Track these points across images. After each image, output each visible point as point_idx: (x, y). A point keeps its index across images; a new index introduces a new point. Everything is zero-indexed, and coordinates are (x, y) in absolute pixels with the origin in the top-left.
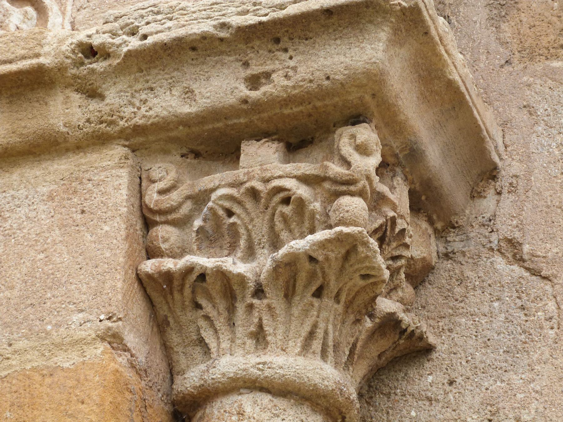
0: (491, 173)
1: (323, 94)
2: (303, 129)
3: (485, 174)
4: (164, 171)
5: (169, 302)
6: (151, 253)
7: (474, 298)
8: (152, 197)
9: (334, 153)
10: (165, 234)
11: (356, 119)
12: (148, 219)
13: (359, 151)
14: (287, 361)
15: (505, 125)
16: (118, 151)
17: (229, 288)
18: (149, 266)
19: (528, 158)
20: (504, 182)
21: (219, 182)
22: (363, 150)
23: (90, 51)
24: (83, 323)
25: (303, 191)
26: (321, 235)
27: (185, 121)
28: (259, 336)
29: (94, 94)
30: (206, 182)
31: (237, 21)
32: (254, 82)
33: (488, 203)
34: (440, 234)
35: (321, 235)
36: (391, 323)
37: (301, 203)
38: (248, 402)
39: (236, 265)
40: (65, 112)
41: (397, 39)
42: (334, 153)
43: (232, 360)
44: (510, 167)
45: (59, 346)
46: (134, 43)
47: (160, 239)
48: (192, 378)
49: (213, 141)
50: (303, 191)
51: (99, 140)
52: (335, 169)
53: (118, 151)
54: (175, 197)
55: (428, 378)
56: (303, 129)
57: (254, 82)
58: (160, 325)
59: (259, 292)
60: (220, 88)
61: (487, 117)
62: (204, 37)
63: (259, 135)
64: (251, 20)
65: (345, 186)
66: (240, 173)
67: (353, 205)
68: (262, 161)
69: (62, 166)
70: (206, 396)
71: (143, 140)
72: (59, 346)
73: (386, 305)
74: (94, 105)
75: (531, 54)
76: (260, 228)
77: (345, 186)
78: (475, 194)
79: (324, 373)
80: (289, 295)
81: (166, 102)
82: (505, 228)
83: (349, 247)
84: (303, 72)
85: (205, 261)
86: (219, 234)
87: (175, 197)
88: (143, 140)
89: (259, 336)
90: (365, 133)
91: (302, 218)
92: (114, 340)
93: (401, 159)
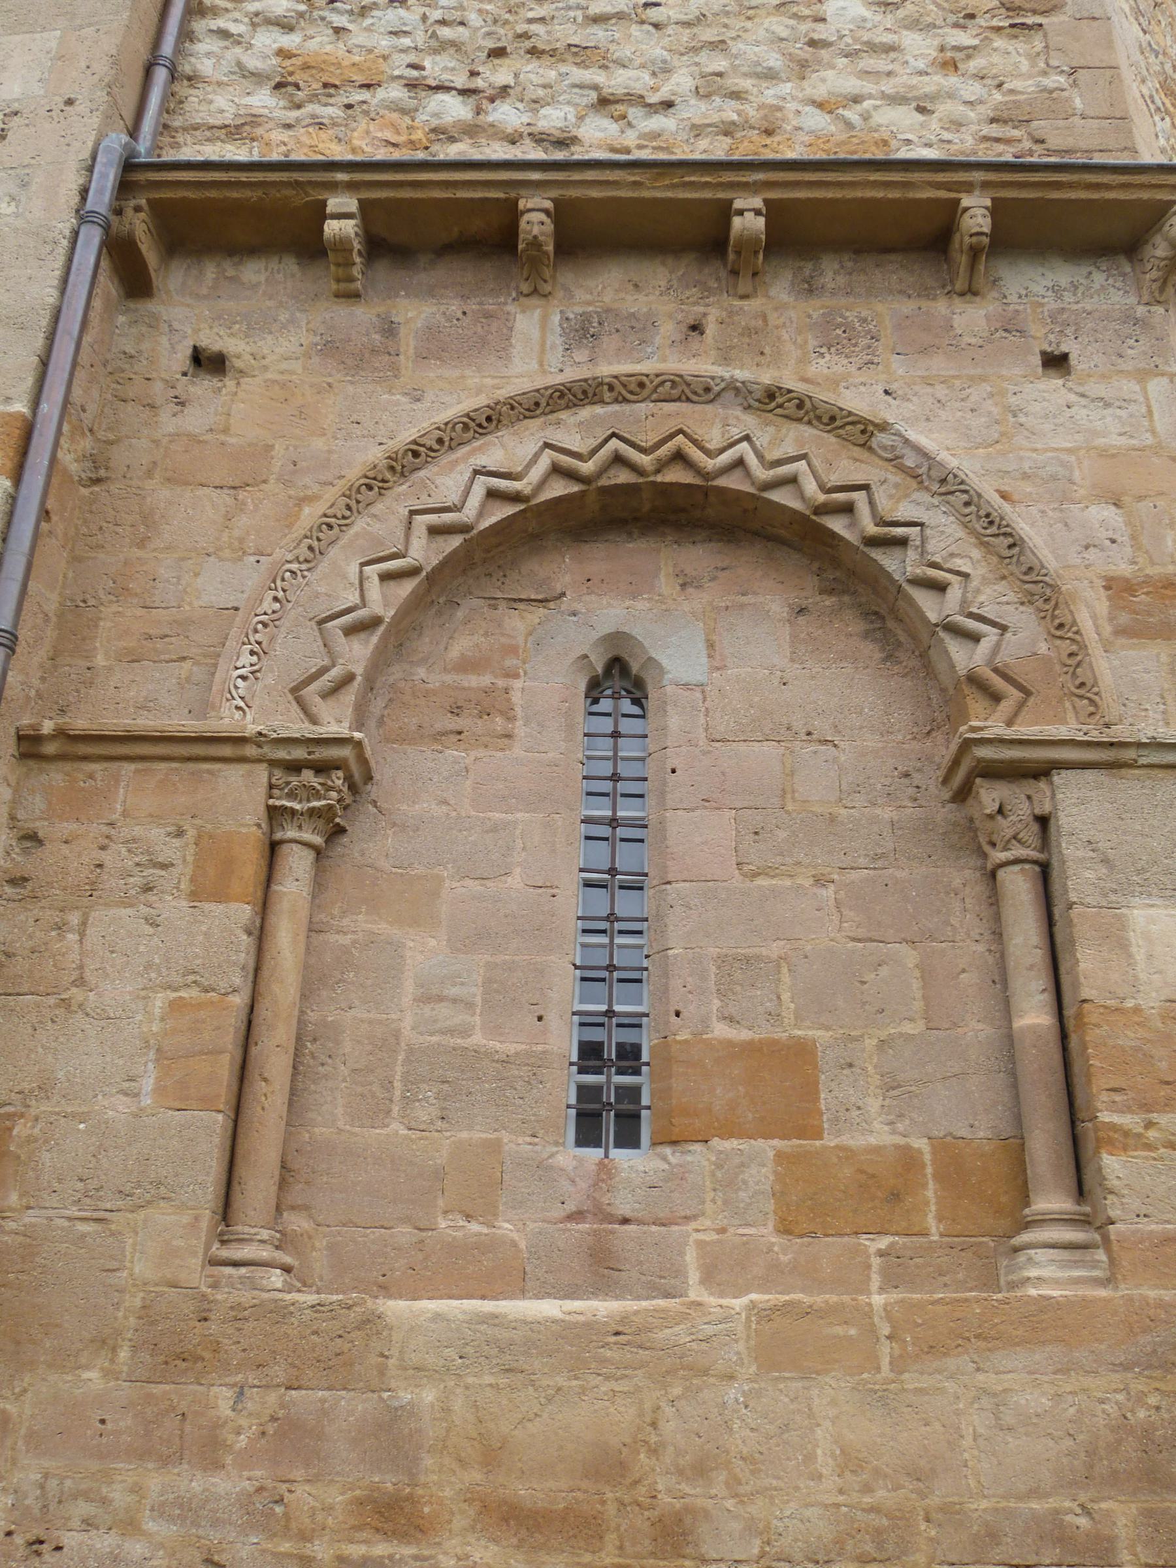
0: (371, 778)
1: (329, 761)
2: (322, 768)
3: (369, 778)
4: (278, 773)
5: (275, 814)
6: (271, 797)
7: (362, 816)
8: (274, 781)
9: (329, 777)
10: (276, 792)
11: (338, 768)
12: (271, 786)
13: (337, 779)
14: (307, 836)
15: (377, 762)
16: (265, 765)
17: (293, 812)
18: (271, 802)
19: (382, 775)
20: (374, 781)
21: (294, 780)
22: (339, 778)
23: (260, 734)
24: (249, 819)
25: (319, 787)
26: (323, 802)
27: (288, 761)
28: (300, 827)
29: (260, 746)
30: (290, 779)
31: (308, 735)
32: (309, 753)
33: (369, 787)
34: (354, 795)
35: (323, 802)
36: (338, 824)
37: (318, 791)
38: (294, 846)
39: (298, 807)
40: (250, 751)
41: (354, 748)
42: (329, 777)
43: (291, 834)
44: (377, 776)
45: (242, 825)
46: (275, 735)
47: (371, 1015)
48: (278, 836)
49: (294, 767)
50: (319, 787)
51: (259, 761)
52: (330, 783)
53: (265, 765)
54: (280, 782)
55: (345, 840)
56: (322, 768)
57: (309, 753)
58: (271, 818)
59: (302, 814)
60: (299, 753)
61: (373, 764)
62: (297, 739)
63: (308, 768)
64: (312, 736)
65: (331, 788)
66: (301, 779)
67: (334, 794)
68: (308, 776)
69: (246, 767)
70: (281, 842)
71: (273, 763)
72: (242, 825)
73: (338, 820)
74: (260, 750)
75: (388, 740)
76: (305, 796)
77: (331, 788)
78: (365, 784)
79: (318, 840)
80: (311, 816)
81: (282, 754)
82: (373, 796)
83: (330, 807)
84: (325, 754)
85: (288, 804)
86: (292, 795)
87: (280, 782)
88: (273, 763)
89: (300, 827)
90: (340, 773)
91: (319, 797)
92: (259, 826)
93: (349, 778)
